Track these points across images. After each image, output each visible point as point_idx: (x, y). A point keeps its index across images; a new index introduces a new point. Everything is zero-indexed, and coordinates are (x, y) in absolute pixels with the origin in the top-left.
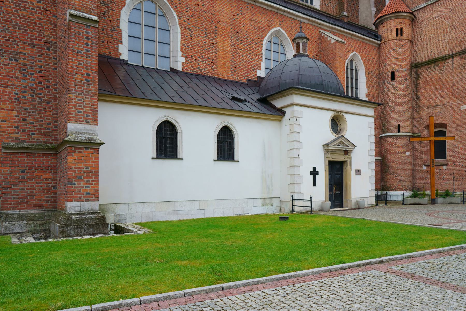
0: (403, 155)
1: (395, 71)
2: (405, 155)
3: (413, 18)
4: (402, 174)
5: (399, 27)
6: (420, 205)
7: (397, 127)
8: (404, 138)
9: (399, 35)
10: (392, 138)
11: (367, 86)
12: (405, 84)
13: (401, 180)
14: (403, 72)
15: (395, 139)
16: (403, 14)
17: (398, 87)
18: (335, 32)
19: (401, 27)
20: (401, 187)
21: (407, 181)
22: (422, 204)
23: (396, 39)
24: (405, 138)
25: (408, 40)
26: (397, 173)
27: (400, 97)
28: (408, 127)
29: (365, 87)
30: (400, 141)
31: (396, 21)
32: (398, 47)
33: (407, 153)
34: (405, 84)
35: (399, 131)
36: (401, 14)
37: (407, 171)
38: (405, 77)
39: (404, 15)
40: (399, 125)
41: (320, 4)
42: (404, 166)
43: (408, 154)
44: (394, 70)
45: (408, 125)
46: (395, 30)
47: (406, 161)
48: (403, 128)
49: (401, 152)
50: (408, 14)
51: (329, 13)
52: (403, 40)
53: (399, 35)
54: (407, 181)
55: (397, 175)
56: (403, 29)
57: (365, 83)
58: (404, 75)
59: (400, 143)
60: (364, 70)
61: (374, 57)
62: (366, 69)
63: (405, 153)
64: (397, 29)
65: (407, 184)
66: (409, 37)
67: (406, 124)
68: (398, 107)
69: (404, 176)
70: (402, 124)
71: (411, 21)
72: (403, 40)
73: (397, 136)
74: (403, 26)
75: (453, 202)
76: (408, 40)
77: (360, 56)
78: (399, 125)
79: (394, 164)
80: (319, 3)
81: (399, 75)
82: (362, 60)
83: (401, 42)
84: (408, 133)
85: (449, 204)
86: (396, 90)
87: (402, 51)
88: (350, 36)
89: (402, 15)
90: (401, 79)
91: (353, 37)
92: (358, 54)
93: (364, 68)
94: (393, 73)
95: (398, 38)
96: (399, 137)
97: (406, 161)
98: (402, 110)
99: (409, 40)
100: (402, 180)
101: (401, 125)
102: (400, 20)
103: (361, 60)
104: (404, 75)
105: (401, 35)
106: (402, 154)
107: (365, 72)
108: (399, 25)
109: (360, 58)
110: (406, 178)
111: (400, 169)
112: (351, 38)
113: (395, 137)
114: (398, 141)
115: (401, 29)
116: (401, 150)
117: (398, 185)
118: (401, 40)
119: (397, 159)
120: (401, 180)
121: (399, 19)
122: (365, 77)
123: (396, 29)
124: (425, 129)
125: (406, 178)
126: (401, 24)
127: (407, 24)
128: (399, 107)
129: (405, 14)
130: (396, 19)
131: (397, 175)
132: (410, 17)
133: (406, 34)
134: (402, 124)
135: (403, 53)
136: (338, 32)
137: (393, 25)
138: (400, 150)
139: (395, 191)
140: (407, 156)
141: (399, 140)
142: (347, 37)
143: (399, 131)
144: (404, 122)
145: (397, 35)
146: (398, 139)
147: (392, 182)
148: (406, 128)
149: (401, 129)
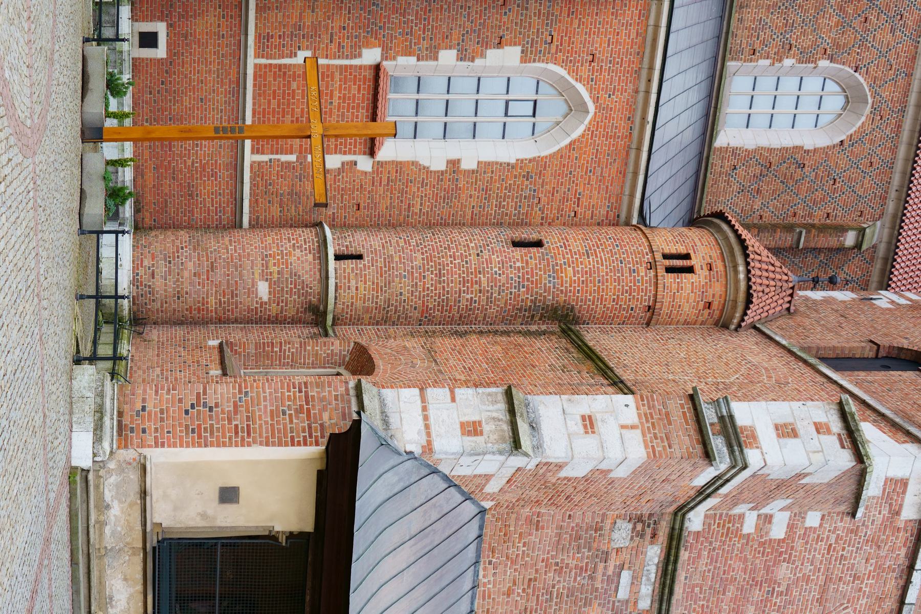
0: (258, 271)
1: (546, 249)
2: (257, 276)
3: (731, 322)
4: (190, 265)
5: (694, 262)
6: (80, 91)
7: (352, 251)
8: (318, 274)
9: (668, 263)
10: (315, 240)
11: (484, 167)
12: (503, 278)
13: (170, 262)
14: (545, 273)
15: (313, 244)
16: (741, 268)
17: (490, 256)
18: (648, 18)
19: (697, 268)
20: (146, 263)
21: (166, 284)
22: (85, 100)
23: (652, 251)
24: (318, 277)
25: (656, 295)
26: (195, 249)
27: (456, 262)
28: (357, 289)
29: (484, 159)
30: (307, 261)
31: (715, 253)
32: (628, 257)
33: (266, 284)
34: (503, 278)
35: (338, 257)
36: (740, 260)
37: (204, 287)
38: (528, 279)
39: (736, 272)
40: (360, 257)
41: (731, 145)
42: (219, 276)
43: (263, 289)
44: (546, 245)
45: (362, 290)
46: (682, 250)
47: (236, 282)
48: (353, 271)
49: (267, 263)
50: (743, 285)
51: (709, 182)
52: (652, 273)
53: (668, 263)
54: (166, 284)
55: (187, 252)
56: (689, 275)
57: (494, 160)
58: (532, 277)
59: (298, 259)
60: (536, 155)
61: (584, 202)
62: (540, 164)
63: (266, 276)
64: (687, 257)
65: (158, 283)
66: (665, 299)
67: (365, 283)
68: (423, 254)
69: (186, 274)
70: (364, 265)
71: (721, 317)
72: (652, 273)
73: (322, 248)
74: (700, 276)
75: (88, 200)
76: (656, 295)
77: (583, 136)
78: (360, 257)
79: (227, 243)
80: (734, 143)
81: (531, 258)
82: (570, 144)
83: (645, 265)
84: (336, 291)
85: (82, 191)
86: (481, 251)
87: (615, 270)
88: (642, 87)
89: (735, 267)
90: (519, 264)
91: (641, 95)
92: (587, 122)
93: (543, 154)
94: (539, 244)
95: (659, 256)
96: (319, 257)
97: (236, 282)
98: (412, 268)
99: (655, 301)
100: (170, 267)
101: (360, 264)
102: (719, 266)
103: (567, 141)
104: (532, 277)
105: (669, 270)
106: (260, 266)
107: (530, 161)
108: (704, 263)
109: (575, 135)
110: (178, 280)
111: (207, 261)
112: (637, 92)
113: (319, 246)
114: (306, 255)
115: (690, 270)
116: (275, 265)
117: (153, 254)
118: (652, 266)
119: (244, 251)
120: (170, 262)
121: (723, 260)
122: (513, 161)
123: (686, 252)
124: (352, 344)
125: (178, 280)
126: (705, 267)
127: (711, 291)
128: (423, 259)
129: (742, 276)
130: (722, 254)
131: (187, 252)
132: (735, 301)
133: (674, 286)
134: (364, 265)
135: (607, 274)
136: (650, 29)
137: (699, 244)
138: (274, 258)
139: (133, 246)
140: (253, 286)
141: (310, 257)
142: (638, 72)
143: (338, 257)
144: (371, 273)
145: (666, 257)
146: (314, 254)
147: (164, 240)
148: (353, 283)
149: (349, 264)
